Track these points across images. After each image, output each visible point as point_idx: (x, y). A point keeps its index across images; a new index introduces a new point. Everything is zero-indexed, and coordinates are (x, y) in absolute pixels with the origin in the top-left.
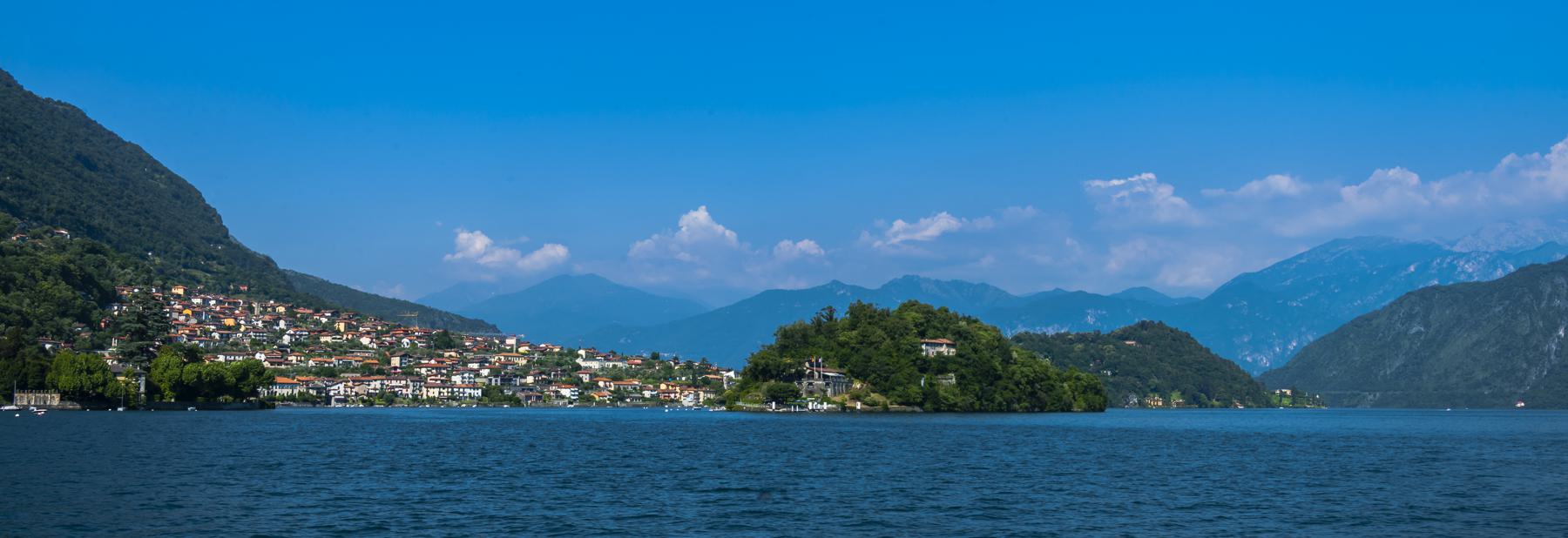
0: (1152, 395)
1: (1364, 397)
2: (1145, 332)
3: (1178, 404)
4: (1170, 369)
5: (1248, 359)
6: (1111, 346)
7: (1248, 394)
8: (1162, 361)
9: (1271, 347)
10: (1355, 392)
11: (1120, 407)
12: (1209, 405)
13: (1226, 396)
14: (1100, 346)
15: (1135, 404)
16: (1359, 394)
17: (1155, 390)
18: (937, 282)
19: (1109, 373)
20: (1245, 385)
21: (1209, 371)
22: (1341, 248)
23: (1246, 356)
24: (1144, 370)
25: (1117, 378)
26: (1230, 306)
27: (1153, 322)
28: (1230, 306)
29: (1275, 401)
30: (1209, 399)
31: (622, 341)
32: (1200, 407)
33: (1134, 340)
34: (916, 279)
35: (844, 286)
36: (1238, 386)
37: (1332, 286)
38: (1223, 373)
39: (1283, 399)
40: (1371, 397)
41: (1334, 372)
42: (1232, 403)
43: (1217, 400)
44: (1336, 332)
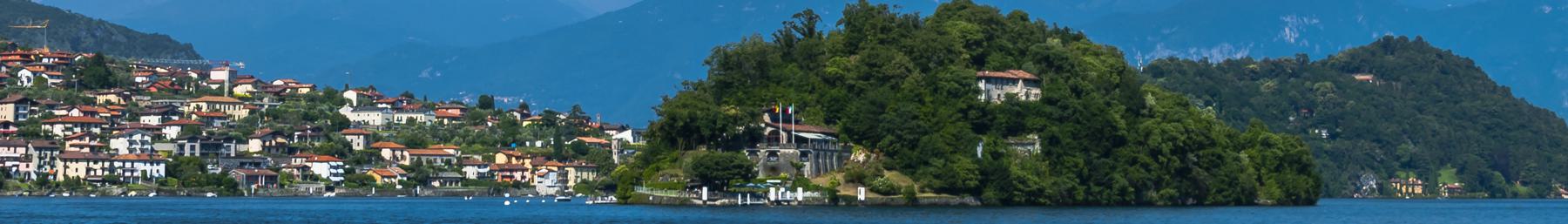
0: (1403, 175)
2: (1391, 58)
3: (1451, 190)
4: (1437, 126)
6: (1328, 84)
8: (1421, 111)
11: (1344, 197)
12: (1509, 194)
14: (1308, 84)
17: (1409, 165)
19: (1324, 134)
21: (1508, 130)
25: (1338, 143)
26: (1548, 9)
28: (1548, 9)
30: (1508, 181)
31: (425, 74)
32: (1493, 196)
33: (1370, 72)
38: (1536, 133)
42: (1550, 189)
43: (1524, 184)
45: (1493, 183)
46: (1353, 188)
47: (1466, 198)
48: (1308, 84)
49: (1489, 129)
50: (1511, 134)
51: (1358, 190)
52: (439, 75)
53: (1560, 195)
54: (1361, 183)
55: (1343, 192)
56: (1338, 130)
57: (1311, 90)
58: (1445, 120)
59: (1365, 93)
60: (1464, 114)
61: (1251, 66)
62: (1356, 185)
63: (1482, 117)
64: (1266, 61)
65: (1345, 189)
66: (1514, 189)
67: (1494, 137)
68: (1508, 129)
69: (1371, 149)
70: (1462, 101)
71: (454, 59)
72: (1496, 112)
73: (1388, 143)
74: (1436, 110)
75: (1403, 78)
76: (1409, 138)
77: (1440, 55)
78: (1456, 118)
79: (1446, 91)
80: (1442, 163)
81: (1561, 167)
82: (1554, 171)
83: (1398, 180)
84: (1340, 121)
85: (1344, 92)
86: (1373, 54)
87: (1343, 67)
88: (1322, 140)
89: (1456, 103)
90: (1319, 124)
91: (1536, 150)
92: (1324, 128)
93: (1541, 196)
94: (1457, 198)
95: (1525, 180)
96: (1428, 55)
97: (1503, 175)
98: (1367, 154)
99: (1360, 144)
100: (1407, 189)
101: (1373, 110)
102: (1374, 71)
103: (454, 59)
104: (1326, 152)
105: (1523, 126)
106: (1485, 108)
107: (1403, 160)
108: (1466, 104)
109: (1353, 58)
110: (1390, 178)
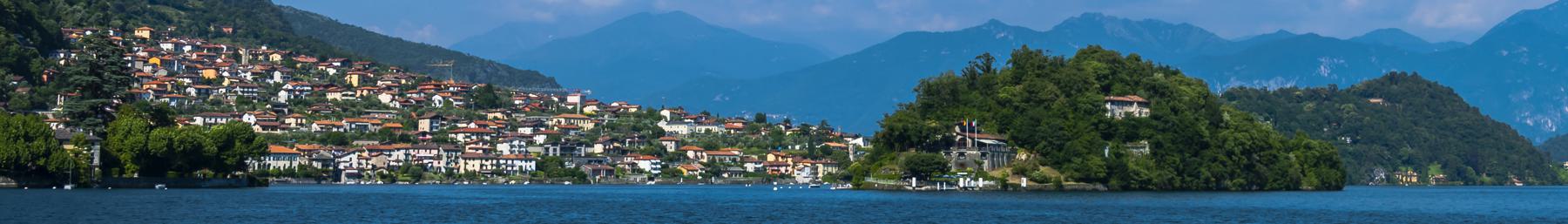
0: (1404, 169)
2: (1395, 87)
3: (1437, 180)
4: (1427, 135)
6: (1351, 105)
7: (1528, 167)
8: (1416, 124)
13: (1500, 170)
14: (1337, 105)
15: (1383, 180)
18: (1126, 23)
20: (1525, 156)
21: (1478, 138)
23: (1526, 118)
24: (1393, 137)
25: (1358, 147)
31: (717, 98)
32: (1466, 184)
33: (1380, 97)
34: (1097, 18)
35: (1004, 27)
36: (1515, 157)
38: (1496, 139)
43: (1488, 175)
46: (1369, 178)
48: (1337, 105)
50: (1479, 140)
51: (1372, 180)
56: (1358, 138)
64: (1307, 89)
73: (1393, 146)
74: (1427, 124)
75: (1403, 101)
78: (1442, 129)
80: (1431, 161)
81: (1514, 163)
86: (1383, 84)
87: (1361, 93)
88: (1347, 144)
89: (1441, 118)
93: (1501, 184)
100: (1406, 179)
104: (1350, 153)
105: (1488, 135)
108: (1448, 119)
109: (1369, 87)
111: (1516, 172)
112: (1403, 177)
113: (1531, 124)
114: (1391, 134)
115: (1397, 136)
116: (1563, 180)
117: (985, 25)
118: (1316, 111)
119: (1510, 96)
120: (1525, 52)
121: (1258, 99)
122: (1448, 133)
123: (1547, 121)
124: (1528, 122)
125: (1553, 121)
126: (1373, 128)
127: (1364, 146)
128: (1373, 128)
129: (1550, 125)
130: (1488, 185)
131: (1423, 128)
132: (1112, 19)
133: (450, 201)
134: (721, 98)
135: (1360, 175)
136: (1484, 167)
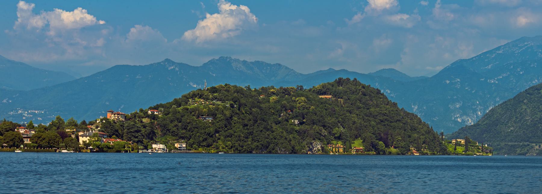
0: (335, 142)
1: (532, 147)
2: (341, 88)
3: (357, 151)
4: (356, 120)
5: (459, 120)
6: (303, 98)
7: (424, 143)
8: (350, 113)
9: (475, 111)
10: (526, 143)
11: (303, 153)
12: (387, 153)
13: (403, 144)
14: (294, 98)
15: (319, 150)
16: (529, 145)
17: (339, 138)
18: (244, 62)
19: (296, 122)
20: (423, 135)
21: (391, 122)
22: (526, 43)
23: (457, 118)
24: (330, 120)
25: (302, 127)
26: (448, 82)
27: (365, 85)
28: (448, 82)
29: (450, 149)
30: (387, 146)
31: (5, 101)
32: (378, 154)
33: (330, 94)
34: (228, 60)
35: (173, 63)
36: (416, 135)
37: (519, 70)
38: (404, 124)
39: (457, 147)
40: (537, 147)
41: (512, 128)
42: (409, 150)
43: (395, 148)
44: (515, 98)
45: (379, 147)
46: (308, 149)
47: (364, 155)
48: (294, 98)
49: (382, 121)
50: (393, 124)
51: (311, 150)
52: (10, 101)
53: (413, 153)
54: (313, 147)
55: (303, 151)
56: (304, 120)
57: (295, 101)
58: (361, 117)
59: (322, 103)
60: (371, 114)
61: (272, 90)
62: (309, 147)
63: (379, 116)
64: (281, 88)
65: (303, 149)
66: (389, 150)
67: (384, 125)
68: (392, 122)
69: (319, 130)
70: (371, 108)
71: (17, 95)
72: (386, 113)
73: (329, 127)
74: (357, 112)
75: (344, 97)
76: (341, 125)
77: (363, 87)
78: (367, 116)
79: (364, 103)
80: (356, 138)
81: (415, 140)
82: (412, 142)
83: (331, 145)
84: (305, 116)
85: (311, 102)
86: (333, 86)
87: (319, 92)
88: (295, 125)
89: (368, 109)
90: (293, 118)
91: (403, 132)
92: (297, 119)
93: (403, 154)
94: (360, 154)
95: (395, 146)
96: (357, 87)
97: (384, 143)
98: (317, 132)
99: (314, 127)
100: (335, 150)
101: (325, 111)
102: (332, 94)
103: (17, 95)
104: (296, 131)
105: (399, 121)
106: (381, 112)
107: (336, 135)
108: (372, 110)
109: (323, 87)
110: (328, 144)
111: (415, 145)
112: (333, 148)
113: (460, 121)
114: (330, 118)
115: (333, 120)
116: (451, 152)
117: (162, 62)
118: (278, 102)
119: (450, 106)
120: (458, 82)
121: (234, 92)
122: (371, 119)
123: (469, 120)
124: (459, 120)
125: (472, 119)
126: (316, 114)
127: (307, 126)
128: (316, 114)
129: (470, 122)
130: (394, 155)
131: (355, 115)
132: (237, 61)
133: (252, 158)
134: (7, 101)
135: (302, 146)
136: (392, 142)
